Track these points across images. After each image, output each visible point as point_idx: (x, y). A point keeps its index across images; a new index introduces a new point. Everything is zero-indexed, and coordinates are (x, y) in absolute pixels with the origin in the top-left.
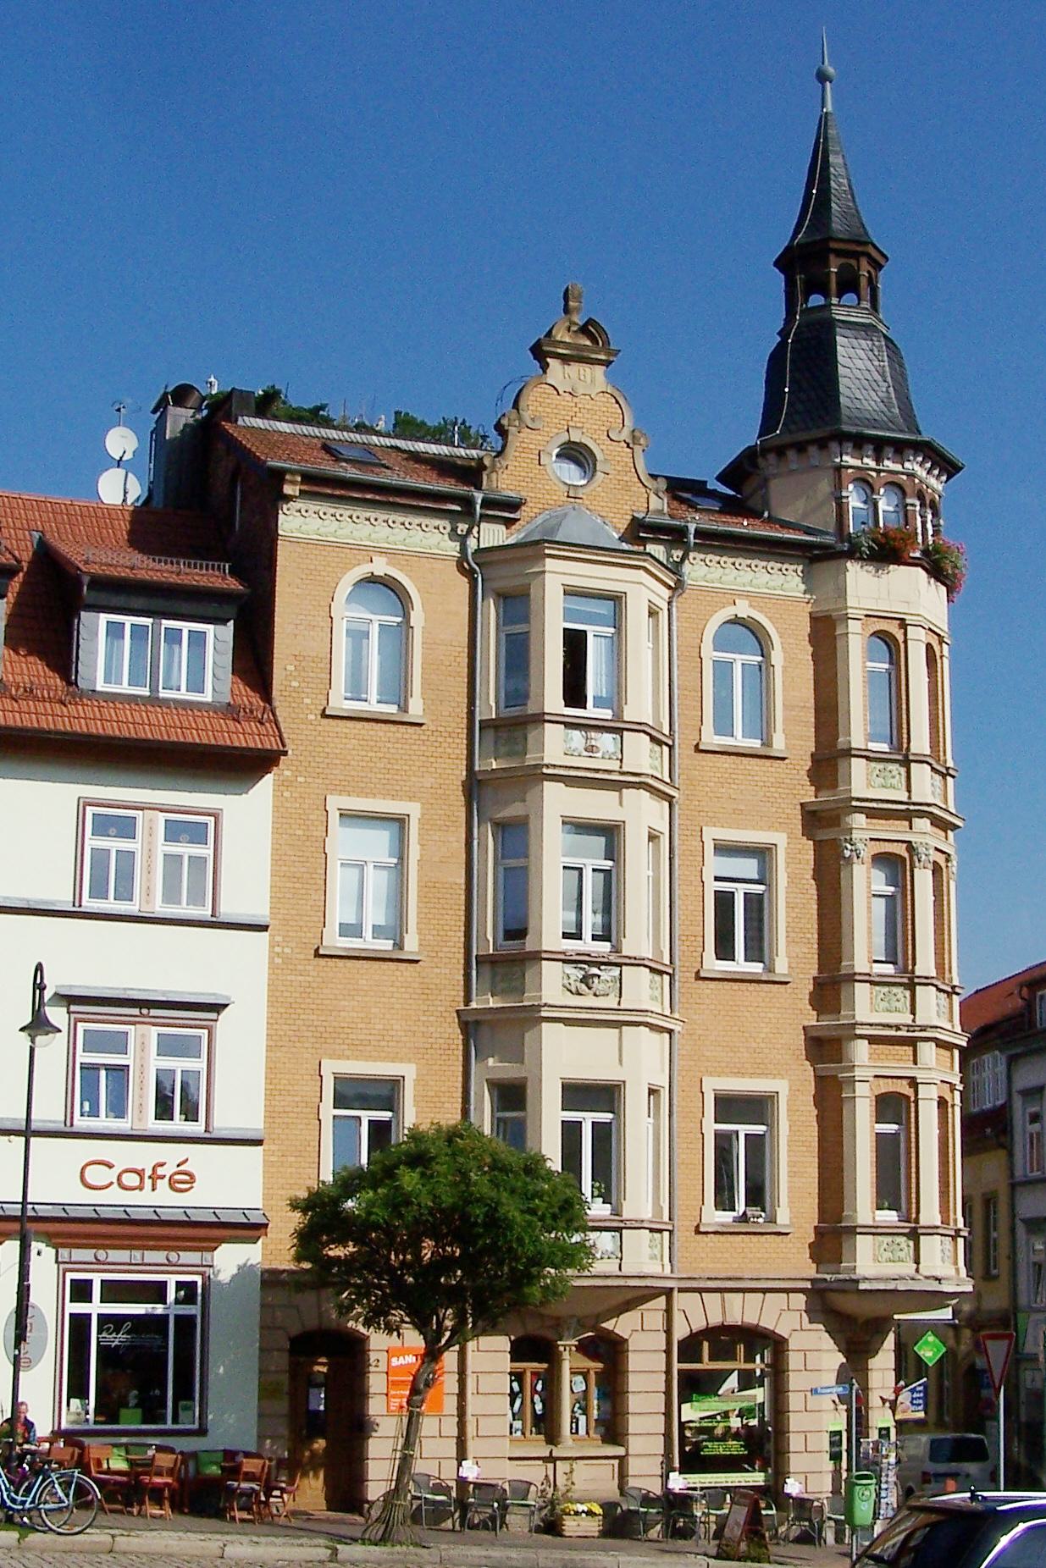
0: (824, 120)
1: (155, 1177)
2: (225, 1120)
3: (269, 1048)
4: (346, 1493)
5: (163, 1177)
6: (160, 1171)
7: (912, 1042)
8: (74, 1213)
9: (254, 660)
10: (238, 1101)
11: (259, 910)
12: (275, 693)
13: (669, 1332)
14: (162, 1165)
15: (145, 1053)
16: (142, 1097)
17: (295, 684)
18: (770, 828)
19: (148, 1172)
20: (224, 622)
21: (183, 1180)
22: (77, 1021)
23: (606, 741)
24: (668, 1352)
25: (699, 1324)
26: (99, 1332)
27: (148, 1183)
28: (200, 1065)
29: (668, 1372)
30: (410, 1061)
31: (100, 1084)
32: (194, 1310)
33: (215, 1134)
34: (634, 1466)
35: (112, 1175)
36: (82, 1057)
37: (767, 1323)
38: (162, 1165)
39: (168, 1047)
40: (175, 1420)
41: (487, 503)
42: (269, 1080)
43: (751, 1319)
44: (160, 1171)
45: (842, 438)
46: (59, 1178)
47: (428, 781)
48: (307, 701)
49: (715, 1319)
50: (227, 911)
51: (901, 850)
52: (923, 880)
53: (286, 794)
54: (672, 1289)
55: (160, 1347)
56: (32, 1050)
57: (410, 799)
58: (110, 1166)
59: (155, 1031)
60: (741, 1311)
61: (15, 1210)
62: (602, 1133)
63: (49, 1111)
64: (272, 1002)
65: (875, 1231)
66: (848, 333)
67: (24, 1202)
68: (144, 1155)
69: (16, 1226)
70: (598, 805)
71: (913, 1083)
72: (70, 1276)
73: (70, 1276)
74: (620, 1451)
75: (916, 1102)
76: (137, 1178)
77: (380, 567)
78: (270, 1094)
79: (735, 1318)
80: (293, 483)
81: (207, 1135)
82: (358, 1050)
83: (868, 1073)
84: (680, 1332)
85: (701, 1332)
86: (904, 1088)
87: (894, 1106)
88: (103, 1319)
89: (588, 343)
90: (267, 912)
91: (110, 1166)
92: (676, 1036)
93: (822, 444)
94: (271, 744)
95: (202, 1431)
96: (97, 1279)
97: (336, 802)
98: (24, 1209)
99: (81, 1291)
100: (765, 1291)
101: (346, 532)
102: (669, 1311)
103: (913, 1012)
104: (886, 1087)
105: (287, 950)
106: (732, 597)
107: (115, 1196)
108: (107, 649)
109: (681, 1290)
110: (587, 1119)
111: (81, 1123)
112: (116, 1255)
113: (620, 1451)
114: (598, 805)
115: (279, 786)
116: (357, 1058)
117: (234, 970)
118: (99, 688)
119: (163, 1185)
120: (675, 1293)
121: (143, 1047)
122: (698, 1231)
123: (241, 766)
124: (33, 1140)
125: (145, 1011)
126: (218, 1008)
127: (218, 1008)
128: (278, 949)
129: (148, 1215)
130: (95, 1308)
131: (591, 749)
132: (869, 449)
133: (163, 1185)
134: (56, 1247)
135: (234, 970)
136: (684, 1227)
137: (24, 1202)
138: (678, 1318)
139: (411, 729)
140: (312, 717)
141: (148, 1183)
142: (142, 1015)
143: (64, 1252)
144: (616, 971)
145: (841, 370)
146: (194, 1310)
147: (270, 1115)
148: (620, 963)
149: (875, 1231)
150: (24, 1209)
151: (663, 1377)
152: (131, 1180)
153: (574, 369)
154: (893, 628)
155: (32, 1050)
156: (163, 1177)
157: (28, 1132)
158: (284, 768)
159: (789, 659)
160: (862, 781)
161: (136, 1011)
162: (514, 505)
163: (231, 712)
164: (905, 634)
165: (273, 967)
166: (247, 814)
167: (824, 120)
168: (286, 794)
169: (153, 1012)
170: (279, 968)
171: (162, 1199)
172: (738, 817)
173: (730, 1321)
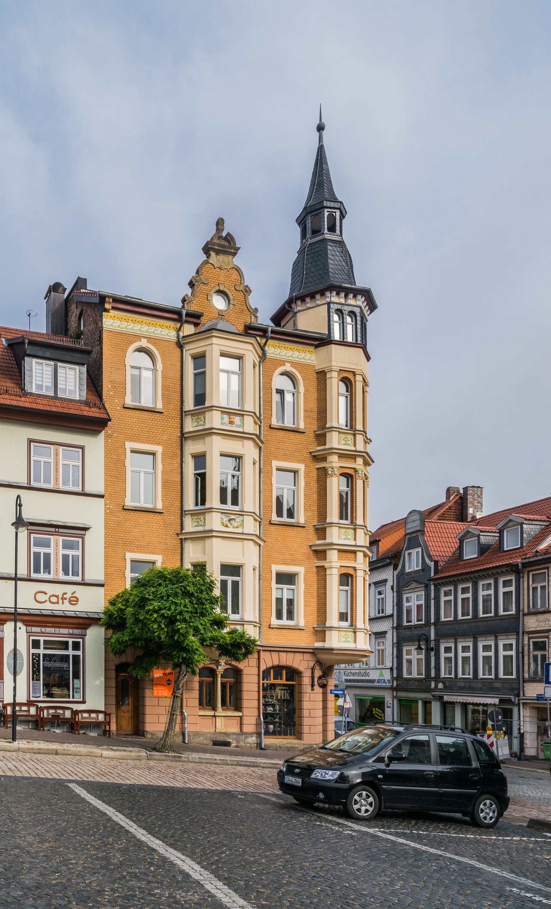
0: (321, 150)
1: (63, 599)
2: (90, 577)
3: (105, 548)
4: (138, 729)
5: (66, 599)
6: (65, 596)
7: (354, 552)
8: (32, 612)
9: (94, 382)
10: (95, 570)
11: (100, 490)
12: (104, 397)
13: (259, 667)
14: (66, 594)
15: (56, 548)
16: (56, 565)
17: (111, 393)
18: (298, 462)
19: (60, 596)
20: (83, 364)
21: (74, 600)
22: (30, 533)
23: (237, 420)
24: (259, 675)
25: (270, 665)
26: (43, 661)
27: (61, 601)
28: (79, 553)
29: (259, 683)
30: (159, 554)
31: (40, 563)
32: (80, 653)
33: (86, 581)
34: (245, 720)
35: (46, 597)
36: (34, 549)
37: (295, 665)
38: (66, 594)
39: (66, 546)
40: (73, 698)
41: (188, 315)
42: (106, 561)
43: (289, 664)
44: (65, 596)
45: (332, 288)
46: (28, 598)
47: (165, 437)
48: (117, 401)
49: (276, 663)
50: (88, 490)
51: (351, 472)
52: (359, 483)
53: (110, 441)
54: (260, 650)
55: (67, 668)
56: (17, 533)
57: (158, 444)
58: (46, 594)
59: (61, 538)
60: (287, 660)
61: (13, 610)
62: (236, 585)
63: (23, 571)
64: (106, 528)
65: (338, 629)
66: (331, 244)
67: (16, 608)
68: (59, 590)
69: (13, 617)
70: (234, 446)
71: (355, 569)
72: (32, 638)
73: (32, 638)
74: (240, 714)
75: (356, 577)
76: (56, 598)
77: (144, 343)
78: (106, 567)
79: (283, 662)
80: (109, 303)
81: (83, 582)
82: (140, 549)
83: (338, 565)
84: (263, 667)
85: (270, 668)
86: (351, 572)
87: (347, 578)
88: (44, 655)
89: (227, 244)
90: (103, 490)
91: (46, 594)
92: (261, 548)
93: (322, 293)
94: (104, 416)
95: (84, 702)
96: (42, 639)
97: (129, 445)
98: (16, 610)
99: (36, 644)
100: (295, 652)
101: (131, 327)
102: (259, 659)
103: (355, 540)
104: (344, 571)
105: (111, 507)
106: (138, 337)
107: (48, 606)
108: (39, 375)
109: (263, 650)
110: (230, 579)
111: (34, 576)
112: (48, 630)
113: (240, 714)
114: (234, 446)
115: (107, 437)
116: (139, 552)
117: (91, 514)
118: (34, 392)
119: (66, 602)
120: (261, 652)
121: (57, 545)
122: (270, 628)
123: (94, 425)
124: (18, 582)
125: (57, 530)
126: (86, 529)
127: (86, 529)
128: (108, 506)
129: (61, 613)
130: (41, 651)
131: (231, 423)
132: (343, 295)
133: (66, 602)
134: (27, 626)
135: (91, 514)
136: (265, 624)
137: (16, 608)
138: (262, 661)
139: (158, 415)
140: (118, 408)
141: (61, 601)
142: (56, 532)
143: (29, 628)
144: (241, 518)
145: (330, 261)
146: (80, 653)
147: (106, 575)
148: (242, 514)
149: (338, 629)
150: (16, 610)
151: (257, 685)
152: (54, 599)
153: (221, 257)
154: (350, 376)
155: (17, 533)
156: (66, 599)
157: (16, 579)
158: (108, 430)
159: (306, 391)
160: (334, 441)
161: (53, 530)
162: (198, 316)
163: (87, 403)
164: (355, 378)
165: (106, 514)
166: (95, 446)
167: (321, 150)
168: (110, 441)
169: (61, 530)
170: (108, 514)
171: (65, 607)
172: (285, 458)
173: (281, 664)
